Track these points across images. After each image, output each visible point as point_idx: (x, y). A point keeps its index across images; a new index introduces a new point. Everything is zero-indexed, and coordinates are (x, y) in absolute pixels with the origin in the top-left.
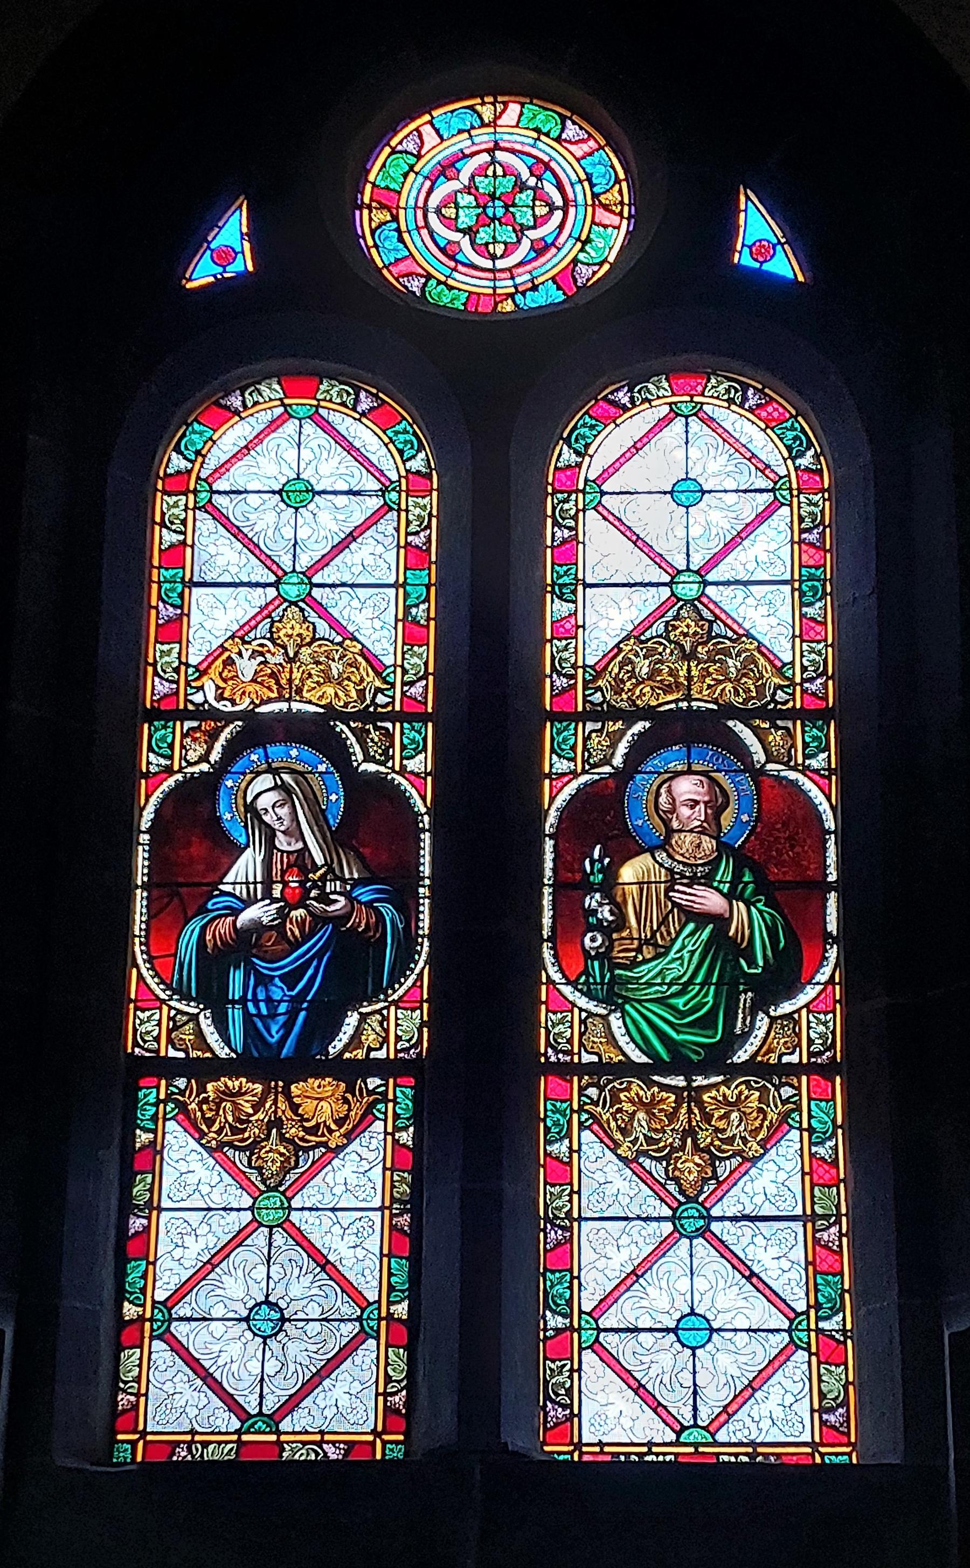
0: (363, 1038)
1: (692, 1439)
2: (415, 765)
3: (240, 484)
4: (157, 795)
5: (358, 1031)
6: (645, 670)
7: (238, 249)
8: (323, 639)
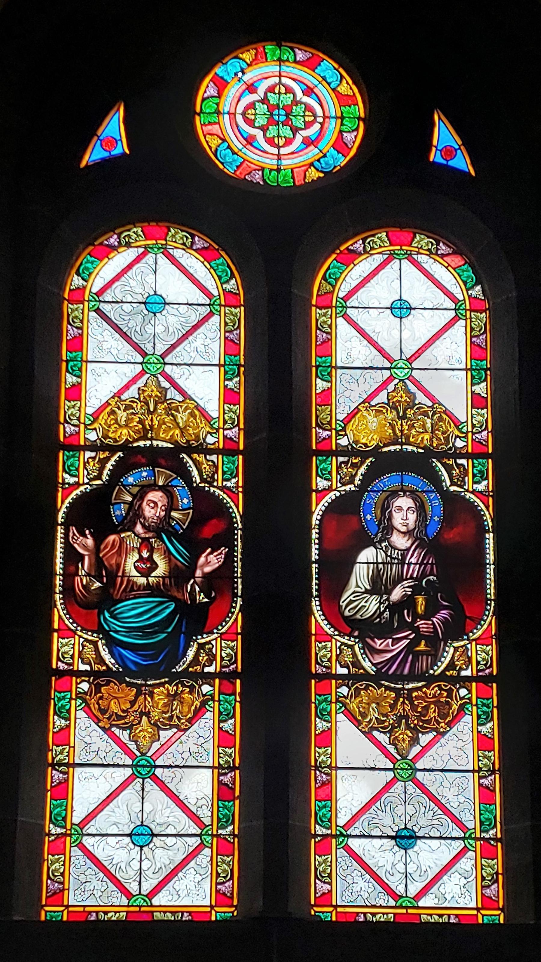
0: (201, 658)
1: (137, 903)
2: (481, 487)
3: (120, 297)
4: (69, 500)
5: (197, 655)
6: (124, 419)
7: (118, 138)
8: (171, 399)
